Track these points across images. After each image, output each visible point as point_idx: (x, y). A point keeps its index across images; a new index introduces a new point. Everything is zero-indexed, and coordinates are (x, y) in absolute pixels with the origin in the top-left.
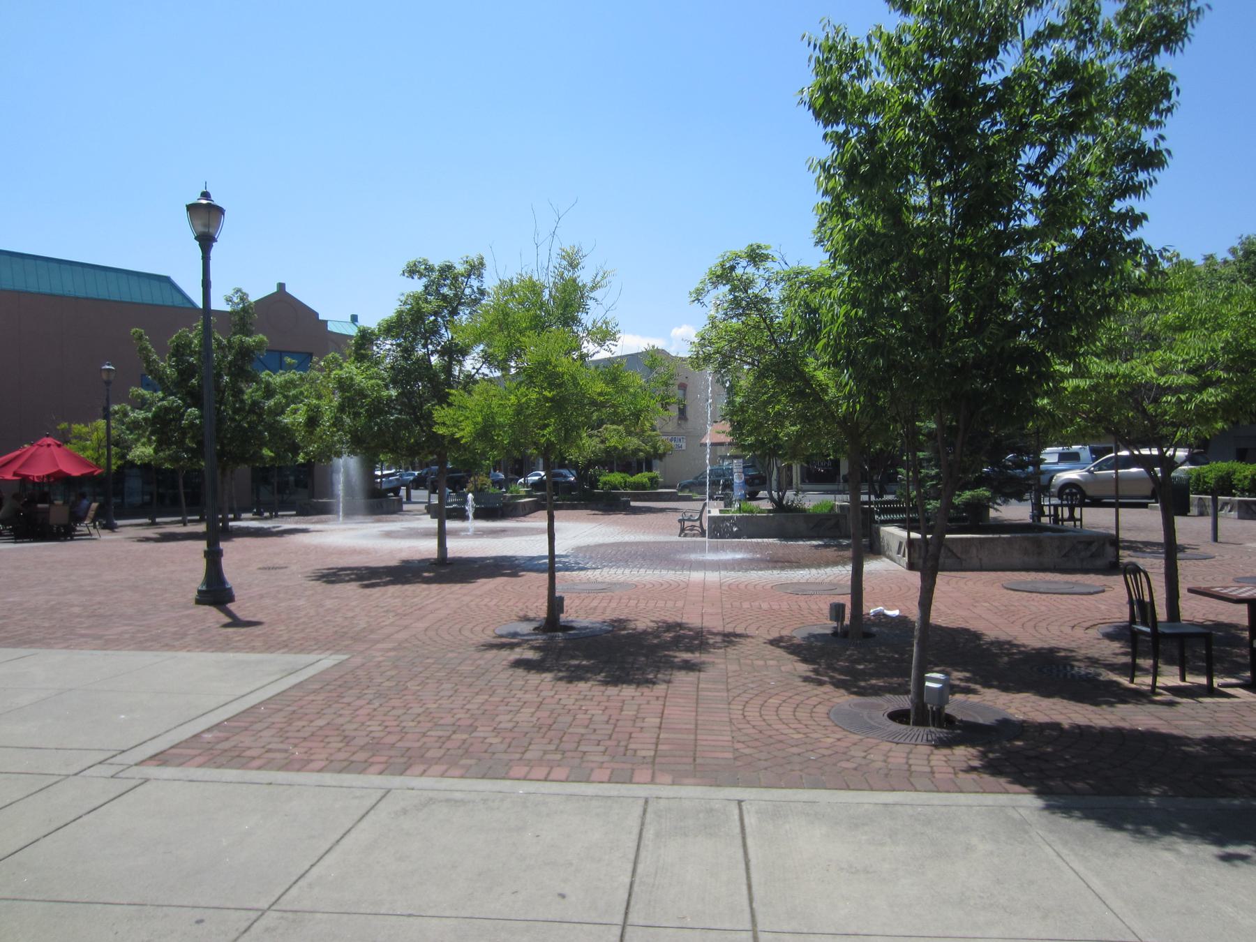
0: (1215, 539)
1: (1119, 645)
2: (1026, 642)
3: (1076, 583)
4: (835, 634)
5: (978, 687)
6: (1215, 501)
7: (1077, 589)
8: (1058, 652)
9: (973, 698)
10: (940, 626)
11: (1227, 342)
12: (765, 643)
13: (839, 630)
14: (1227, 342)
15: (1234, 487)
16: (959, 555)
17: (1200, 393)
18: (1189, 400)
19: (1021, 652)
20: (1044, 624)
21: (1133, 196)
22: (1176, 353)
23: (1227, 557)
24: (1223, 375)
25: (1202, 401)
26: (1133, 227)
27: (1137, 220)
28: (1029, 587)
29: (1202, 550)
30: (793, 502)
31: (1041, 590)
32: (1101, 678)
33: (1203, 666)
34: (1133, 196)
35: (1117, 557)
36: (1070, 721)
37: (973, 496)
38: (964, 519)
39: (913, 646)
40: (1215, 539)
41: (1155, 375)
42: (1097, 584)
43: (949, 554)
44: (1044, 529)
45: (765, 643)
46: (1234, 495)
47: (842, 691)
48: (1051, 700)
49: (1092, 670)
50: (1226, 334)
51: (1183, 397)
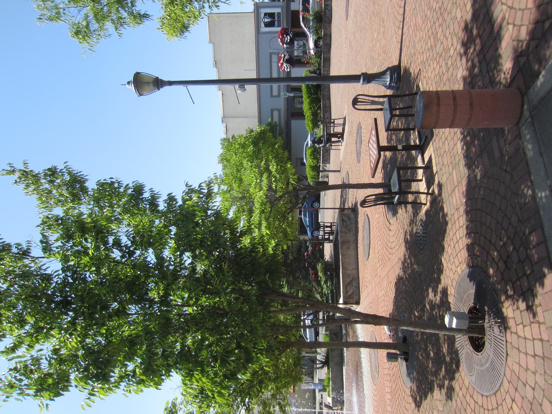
0: (339, 171)
1: (400, 210)
2: (402, 254)
3: (363, 227)
4: (406, 360)
5: (440, 287)
6: (322, 171)
7: (367, 226)
8: (407, 239)
9: (451, 291)
10: (395, 297)
11: (248, 161)
12: (418, 411)
13: (403, 357)
14: (248, 161)
15: (316, 166)
16: (351, 279)
17: (272, 172)
18: (275, 177)
19: (409, 257)
20: (389, 244)
21: (158, 200)
22: (252, 183)
23: (347, 166)
24: (263, 162)
25: (275, 171)
26: (175, 200)
27: (171, 199)
28: (367, 248)
29: (344, 176)
30: (323, 356)
31: (368, 242)
32: (424, 219)
33: (410, 172)
34: (158, 200)
35: (349, 209)
36: (464, 238)
37: (321, 272)
38: (331, 274)
39: (425, 332)
40: (339, 171)
41: (262, 192)
42: (363, 218)
43: (351, 284)
44: (336, 238)
45: (418, 411)
46: (320, 166)
47: (457, 375)
48: (446, 246)
49: (419, 223)
50: (245, 162)
51: (273, 179)
